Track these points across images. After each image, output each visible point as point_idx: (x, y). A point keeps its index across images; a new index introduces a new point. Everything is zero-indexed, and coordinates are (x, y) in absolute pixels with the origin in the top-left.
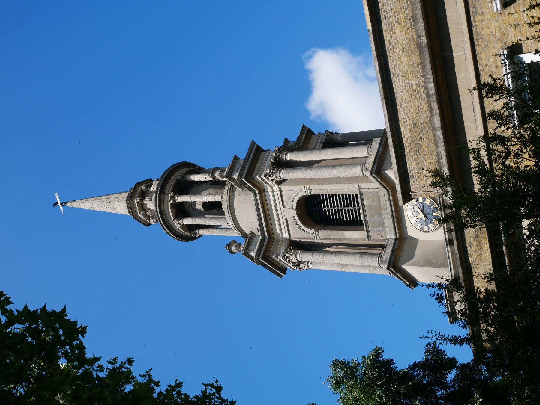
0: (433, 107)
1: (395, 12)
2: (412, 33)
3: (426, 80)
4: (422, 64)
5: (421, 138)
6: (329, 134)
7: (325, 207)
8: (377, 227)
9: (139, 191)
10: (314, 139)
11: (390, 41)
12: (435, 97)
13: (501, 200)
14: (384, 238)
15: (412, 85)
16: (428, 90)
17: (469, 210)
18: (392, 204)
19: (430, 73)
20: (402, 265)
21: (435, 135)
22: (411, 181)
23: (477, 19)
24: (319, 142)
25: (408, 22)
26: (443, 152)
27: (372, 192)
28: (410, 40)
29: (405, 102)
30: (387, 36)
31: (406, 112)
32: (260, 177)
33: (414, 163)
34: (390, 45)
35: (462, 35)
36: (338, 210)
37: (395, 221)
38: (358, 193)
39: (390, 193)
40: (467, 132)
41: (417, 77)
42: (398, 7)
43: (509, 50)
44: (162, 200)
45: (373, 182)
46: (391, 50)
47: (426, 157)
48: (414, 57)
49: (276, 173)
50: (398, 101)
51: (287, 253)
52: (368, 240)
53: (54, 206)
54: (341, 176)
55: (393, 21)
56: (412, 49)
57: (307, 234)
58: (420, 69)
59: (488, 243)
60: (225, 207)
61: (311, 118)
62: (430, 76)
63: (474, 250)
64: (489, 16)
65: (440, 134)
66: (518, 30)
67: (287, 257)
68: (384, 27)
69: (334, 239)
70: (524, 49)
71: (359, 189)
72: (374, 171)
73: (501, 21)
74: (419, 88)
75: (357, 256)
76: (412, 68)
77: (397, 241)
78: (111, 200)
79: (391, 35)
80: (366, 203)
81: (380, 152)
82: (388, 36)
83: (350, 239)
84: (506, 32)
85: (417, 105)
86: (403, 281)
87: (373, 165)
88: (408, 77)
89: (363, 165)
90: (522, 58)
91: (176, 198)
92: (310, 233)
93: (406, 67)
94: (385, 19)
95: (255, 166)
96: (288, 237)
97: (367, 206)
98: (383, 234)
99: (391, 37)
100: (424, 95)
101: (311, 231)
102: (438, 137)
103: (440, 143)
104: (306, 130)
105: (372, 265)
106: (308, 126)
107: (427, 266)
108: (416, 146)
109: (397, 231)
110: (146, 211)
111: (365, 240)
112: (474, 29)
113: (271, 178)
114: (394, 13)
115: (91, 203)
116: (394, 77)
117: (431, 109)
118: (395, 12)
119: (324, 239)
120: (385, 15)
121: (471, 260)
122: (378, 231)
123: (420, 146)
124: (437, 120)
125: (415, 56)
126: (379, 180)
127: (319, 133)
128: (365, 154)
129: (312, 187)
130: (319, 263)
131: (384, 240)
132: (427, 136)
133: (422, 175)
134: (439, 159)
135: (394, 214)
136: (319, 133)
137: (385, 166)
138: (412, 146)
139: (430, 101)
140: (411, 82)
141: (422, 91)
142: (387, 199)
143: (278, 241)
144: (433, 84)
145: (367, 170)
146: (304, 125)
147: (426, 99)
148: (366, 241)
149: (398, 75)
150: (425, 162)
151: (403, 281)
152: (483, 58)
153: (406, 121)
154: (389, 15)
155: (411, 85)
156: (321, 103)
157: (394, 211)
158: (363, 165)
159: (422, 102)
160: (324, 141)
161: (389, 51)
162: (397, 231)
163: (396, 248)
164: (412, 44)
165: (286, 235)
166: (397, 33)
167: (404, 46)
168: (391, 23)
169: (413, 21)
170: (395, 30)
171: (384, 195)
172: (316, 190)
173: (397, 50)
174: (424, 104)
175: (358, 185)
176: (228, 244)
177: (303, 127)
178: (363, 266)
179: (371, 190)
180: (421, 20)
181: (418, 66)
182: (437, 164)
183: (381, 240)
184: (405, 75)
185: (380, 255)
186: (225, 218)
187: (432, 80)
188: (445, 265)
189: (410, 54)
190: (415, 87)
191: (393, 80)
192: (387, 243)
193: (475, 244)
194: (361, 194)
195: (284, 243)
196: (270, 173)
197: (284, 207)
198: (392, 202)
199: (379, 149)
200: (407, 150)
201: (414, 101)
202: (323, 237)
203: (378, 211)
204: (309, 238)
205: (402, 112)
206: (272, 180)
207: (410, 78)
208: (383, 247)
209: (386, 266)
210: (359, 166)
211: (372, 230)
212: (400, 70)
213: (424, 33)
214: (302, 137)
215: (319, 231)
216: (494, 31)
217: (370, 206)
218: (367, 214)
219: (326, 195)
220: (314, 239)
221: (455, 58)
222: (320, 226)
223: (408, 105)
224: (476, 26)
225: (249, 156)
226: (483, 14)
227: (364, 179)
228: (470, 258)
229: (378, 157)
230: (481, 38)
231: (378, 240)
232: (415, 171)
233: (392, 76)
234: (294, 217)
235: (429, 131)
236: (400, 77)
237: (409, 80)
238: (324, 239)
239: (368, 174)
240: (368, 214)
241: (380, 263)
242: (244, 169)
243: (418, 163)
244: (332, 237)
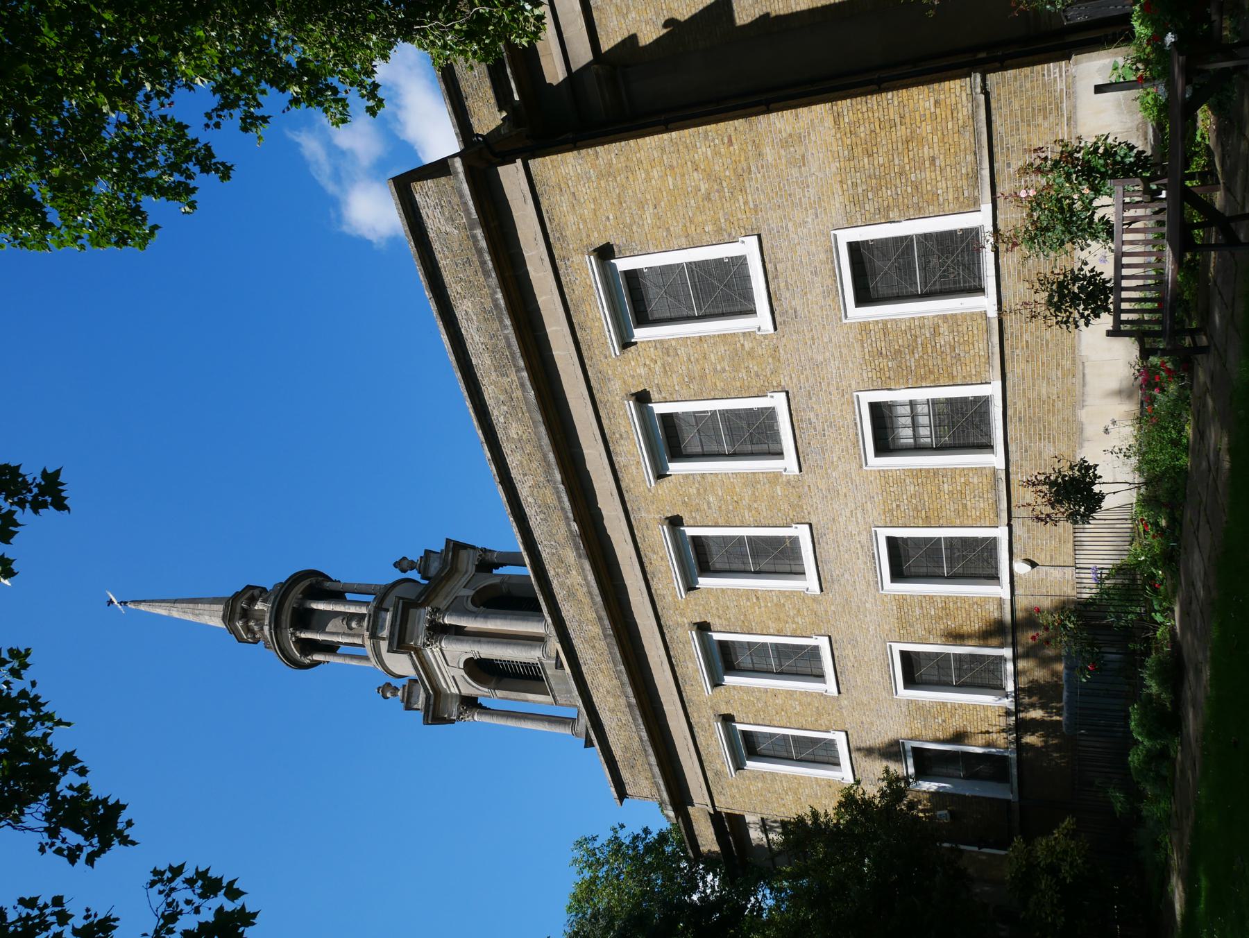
9: (238, 610)
30: (588, 678)
44: (279, 635)
49: (435, 642)
53: (109, 605)
65: (656, 770)
90: (614, 264)
91: (298, 635)
95: (406, 628)
96: (458, 692)
112: (684, 694)
143: (447, 695)
165: (454, 690)
176: (381, 685)
180: (628, 685)
195: (454, 700)
197: (448, 665)
214: (448, 556)
225: (396, 617)
234: (463, 676)
242: (393, 635)
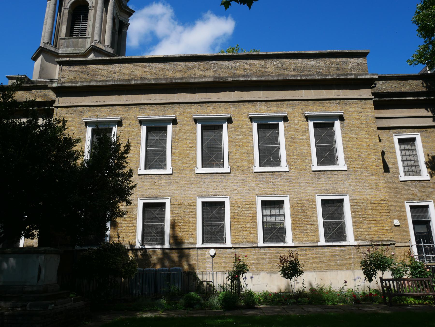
0: (101, 82)
1: (151, 71)
2: (139, 77)
3: (114, 81)
4: (124, 80)
5: (88, 75)
6: (128, 25)
7: (83, 16)
8: (66, 44)
10: (126, 16)
11: (138, 66)
12: (105, 84)
14: (60, 47)
15: (115, 74)
16: (109, 81)
18: (77, 54)
19: (117, 83)
20: (94, 54)
21: (87, 81)
22: (68, 67)
23: (137, 108)
24: (124, 19)
25: (144, 76)
26: (78, 85)
27: (85, 44)
28: (136, 76)
29: (107, 69)
30: (141, 64)
31: (103, 69)
33: (77, 69)
34: (136, 66)
35: (132, 101)
36: (80, 24)
37: (68, 55)
38: (86, 37)
39: (83, 54)
40: (87, 97)
41: (118, 76)
42: (153, 72)
43: (120, 120)
46: (133, 66)
47: (79, 76)
48: (128, 76)
50: (108, 66)
52: (60, 38)
54: (95, 29)
55: (339, 61)
56: (132, 76)
57: (67, 3)
58: (121, 78)
59: (41, 100)
61: (209, 12)
62: (116, 83)
63: (39, 93)
64: (137, 114)
65: (87, 84)
66: (128, 125)
68: (145, 64)
70: (119, 127)
71: (88, 37)
72: (94, 47)
73: (134, 119)
74: (112, 77)
75: (50, 30)
76: (123, 75)
77: (56, 54)
79: (141, 67)
80: (80, 40)
81: (104, 52)
82: (141, 65)
83: (61, 28)
84: (128, 120)
85: (105, 75)
86: (35, 54)
87: (97, 47)
88: (119, 72)
89: (99, 42)
92: (67, 5)
93: (124, 72)
94: (149, 65)
98: (62, 47)
99: (139, 67)
100: (109, 79)
101: (69, 6)
102: (86, 83)
103: (82, 83)
104: (132, 13)
105: (45, 38)
107: (41, 68)
108: (85, 71)
109: (63, 55)
111: (60, 36)
112: (133, 106)
114: (151, 70)
116: (120, 65)
117: (100, 81)
118: (151, 71)
119: (63, 12)
120: (151, 65)
121: (34, 91)
122: (64, 44)
123: (84, 73)
124: (94, 84)
125: (128, 77)
126: (89, 49)
127: (129, 20)
128: (106, 43)
129: (93, 11)
130: (49, 7)
131: (59, 48)
132: (88, 78)
133: (70, 72)
134: (75, 82)
135: (71, 54)
136: (129, 20)
137: (96, 53)
138: (85, 70)
139: (104, 82)
140: (116, 73)
141: (111, 78)
142: (80, 52)
144: (111, 84)
145: (95, 43)
147: (106, 80)
148: (60, 36)
149: (121, 67)
150: (76, 75)
151: (35, 54)
152: (119, 109)
153: (98, 68)
154: (150, 67)
155: (115, 73)
156: (208, 19)
157: (73, 54)
158: (99, 42)
159: (106, 78)
160: (124, 21)
161: (133, 64)
162: (63, 55)
163: (53, 53)
164: (134, 76)
166: (140, 70)
167: (134, 73)
168: (146, 68)
169: (144, 78)
170: (142, 69)
171: (83, 50)
172: (91, 13)
173: (133, 69)
174: (104, 78)
175: (90, 37)
177: (133, 11)
179: (87, 44)
180: (142, 82)
181: (123, 78)
182: (74, 81)
183: (59, 45)
184: (120, 71)
185: (50, 44)
187: (113, 84)
188: (40, 77)
189: (129, 75)
190: (113, 75)
191: (119, 65)
192: (57, 48)
193: (41, 94)
194: (85, 38)
198: (78, 54)
199: (107, 51)
200: (84, 66)
201: (107, 74)
202: (64, 13)
203: (75, 46)
204: (65, 4)
205: (103, 67)
207: (118, 73)
208: (56, 46)
210: (99, 39)
211: (65, 41)
212: (123, 69)
213: (136, 83)
215: (68, 11)
216: (131, 115)
217: (78, 42)
218: (74, 40)
219: (87, 18)
220: (64, 7)
221: (122, 96)
223: (106, 70)
224: (135, 107)
226: (139, 111)
227: (92, 41)
228: (35, 91)
229: (101, 50)
230: (129, 109)
231: (59, 44)
232: (72, 69)
233: (121, 64)
235: (91, 79)
236: (120, 68)
237: (117, 72)
238: (63, 12)
240: (74, 40)
241: (45, 43)
243: (76, 71)
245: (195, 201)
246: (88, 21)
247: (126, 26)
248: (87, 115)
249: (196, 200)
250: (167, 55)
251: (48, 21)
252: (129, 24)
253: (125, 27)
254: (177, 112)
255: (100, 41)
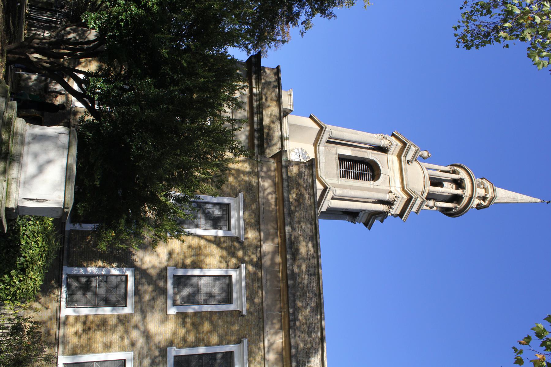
6: (354, 221)
10: (364, 220)
13: (94, 169)
14: (326, 148)
17: (136, 163)
24: (361, 217)
32: (403, 198)
45: (330, 183)
51: (390, 146)
60: (428, 182)
67: (390, 143)
69: (361, 151)
78: (508, 199)
97: (67, 231)
104: (368, 226)
106: (367, 229)
107: (301, 126)
110: (484, 188)
113: (395, 195)
115: (522, 199)
127: (360, 223)
131: (325, 146)
136: (360, 223)
146: (370, 230)
160: (358, 217)
178: (340, 131)
186: (429, 175)
196: (395, 198)
206: (395, 194)
208: (328, 142)
209: (327, 129)
222: (367, 161)
239: (332, 188)
244: (360, 152)
245: (126, 349)
246: (357, 180)
247: (353, 220)
248: (247, 197)
249: (128, 351)
250: (322, 278)
251: (355, 135)
252: (355, 224)
253: (352, 219)
254: (250, 317)
255: (335, 196)
